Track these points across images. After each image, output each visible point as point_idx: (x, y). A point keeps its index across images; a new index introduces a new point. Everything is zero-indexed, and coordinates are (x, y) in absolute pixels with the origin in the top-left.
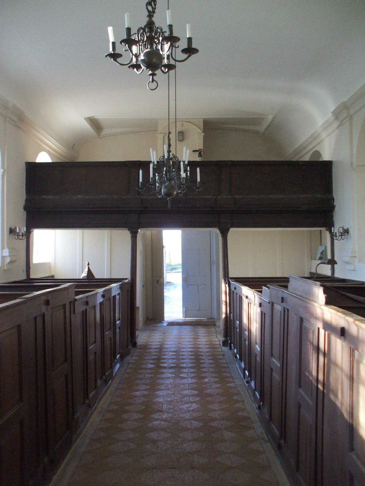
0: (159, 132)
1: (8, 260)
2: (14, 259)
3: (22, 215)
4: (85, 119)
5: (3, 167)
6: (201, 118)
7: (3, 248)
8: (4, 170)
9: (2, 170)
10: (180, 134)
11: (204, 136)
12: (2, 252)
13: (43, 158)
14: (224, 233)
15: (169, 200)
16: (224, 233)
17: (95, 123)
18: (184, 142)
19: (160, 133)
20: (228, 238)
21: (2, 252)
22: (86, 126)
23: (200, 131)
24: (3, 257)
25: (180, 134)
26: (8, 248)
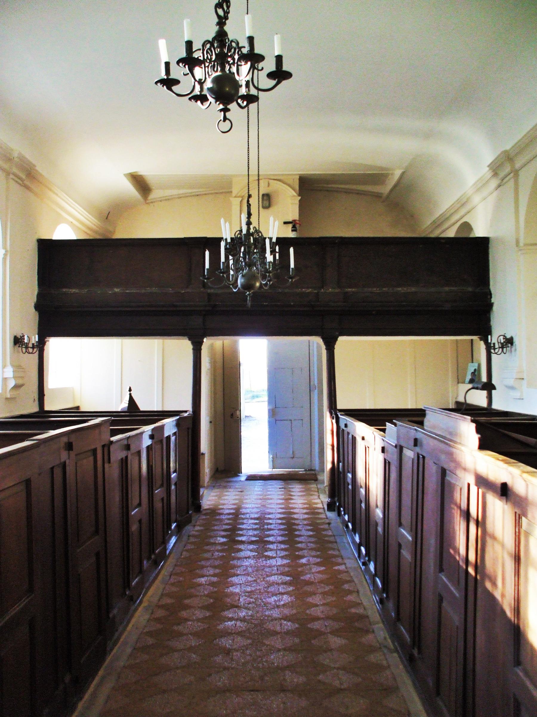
0: (234, 194)
2: (20, 382)
4: (126, 175)
5: (4, 247)
7: (4, 366)
11: (300, 201)
12: (3, 372)
19: (235, 197)
21: (3, 372)
23: (295, 194)
24: (5, 380)
25: (265, 198)
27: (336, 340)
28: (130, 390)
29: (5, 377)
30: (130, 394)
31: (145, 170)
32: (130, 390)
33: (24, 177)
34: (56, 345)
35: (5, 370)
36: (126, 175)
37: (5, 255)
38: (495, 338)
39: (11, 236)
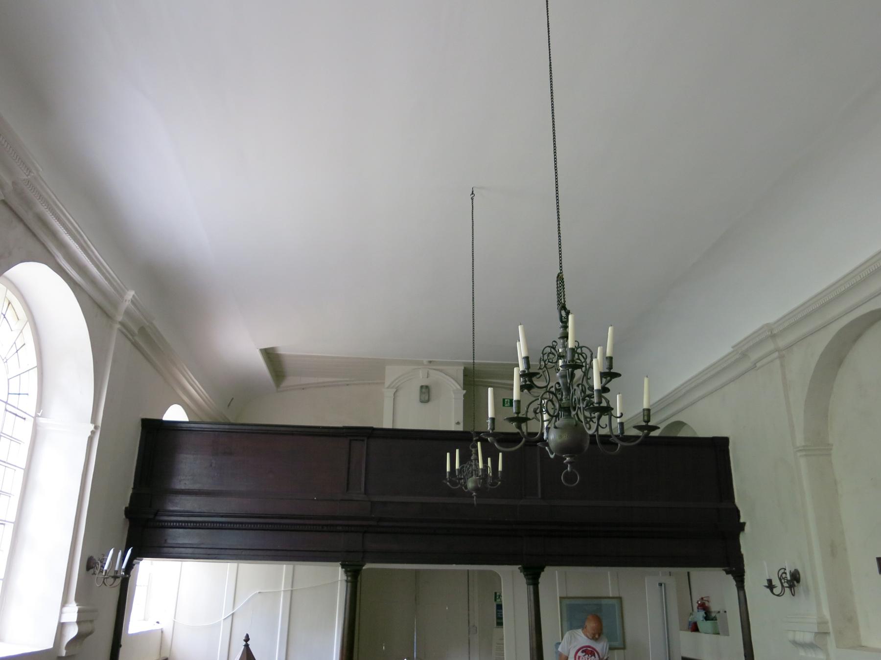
0: (387, 384)
1: (72, 632)
2: (87, 627)
3: (119, 525)
4: (261, 350)
5: (94, 420)
6: (458, 364)
7: (65, 602)
8: (96, 427)
9: (92, 427)
10: (424, 390)
11: (464, 396)
12: (61, 613)
13: (175, 414)
14: (533, 576)
15: (568, 462)
16: (533, 576)
17: (270, 355)
18: (430, 404)
19: (388, 388)
20: (540, 580)
21: (61, 613)
22: (260, 363)
23: (459, 387)
24: (61, 626)
25: (424, 390)
26: (77, 600)
27: (542, 569)
28: (247, 639)
29: (63, 621)
30: (247, 646)
31: (288, 344)
32: (247, 639)
33: (136, 331)
34: (151, 572)
35: (65, 609)
36: (261, 350)
37: (93, 433)
38: (756, 574)
39: (114, 361)
